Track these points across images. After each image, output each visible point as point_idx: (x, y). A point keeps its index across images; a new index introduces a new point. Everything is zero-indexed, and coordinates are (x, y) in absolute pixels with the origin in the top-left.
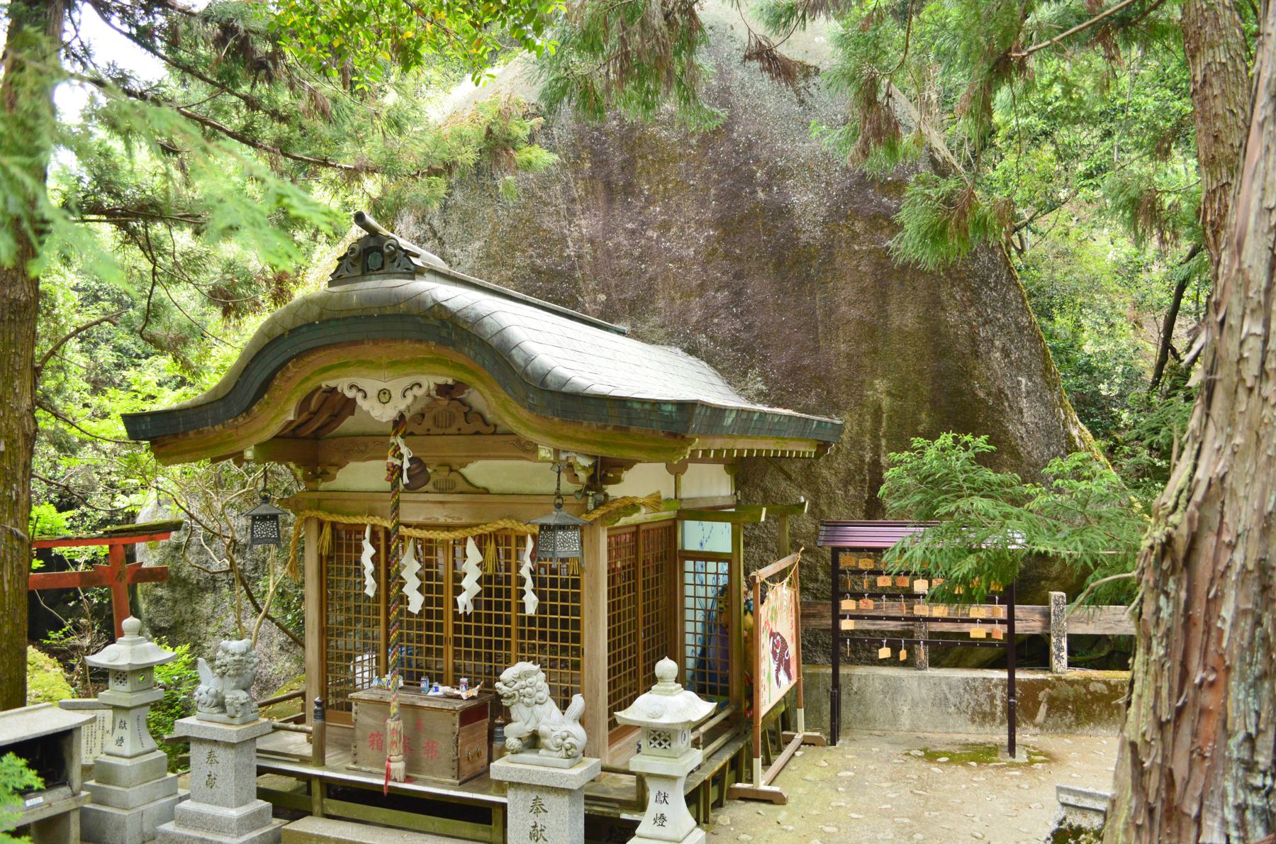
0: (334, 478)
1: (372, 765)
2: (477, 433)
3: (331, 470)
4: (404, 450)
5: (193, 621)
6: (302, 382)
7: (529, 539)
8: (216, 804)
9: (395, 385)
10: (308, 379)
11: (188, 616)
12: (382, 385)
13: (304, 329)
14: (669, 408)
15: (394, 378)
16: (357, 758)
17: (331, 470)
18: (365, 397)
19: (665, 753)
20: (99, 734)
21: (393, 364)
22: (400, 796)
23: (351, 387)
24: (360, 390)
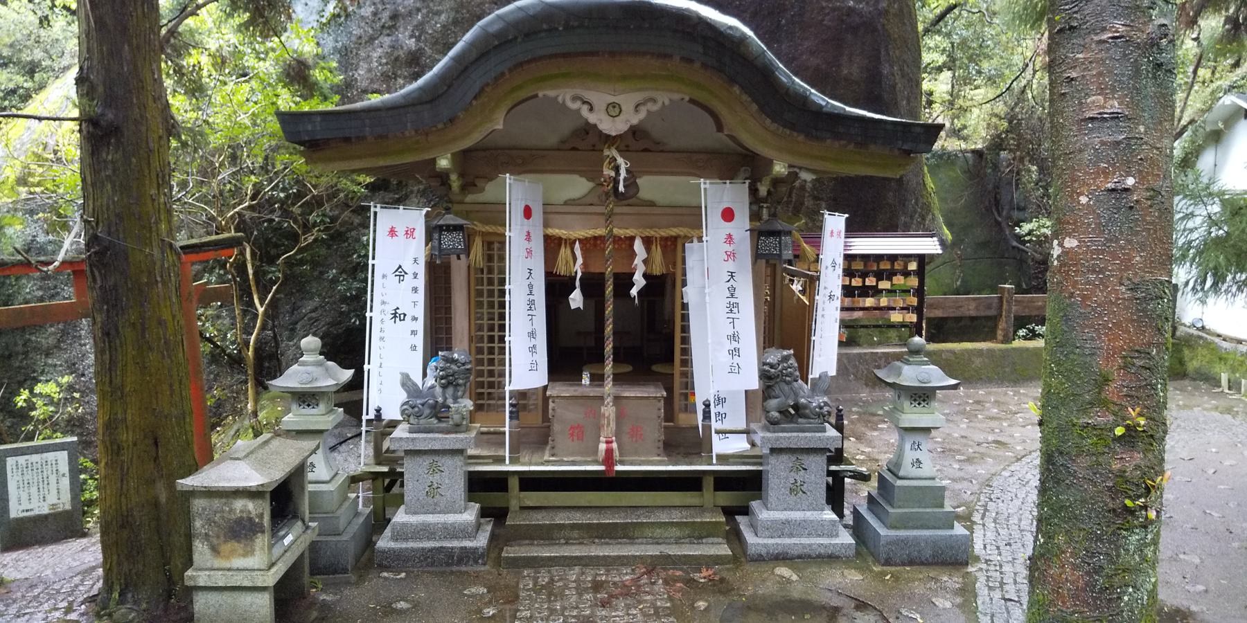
0: (482, 190)
1: (572, 455)
2: (646, 150)
3: (479, 183)
4: (620, 160)
5: (26, 353)
6: (514, 90)
7: (638, 246)
8: (439, 513)
9: (627, 100)
10: (520, 87)
11: (20, 348)
12: (611, 99)
13: (543, 34)
14: (918, 130)
15: (624, 92)
16: (555, 451)
17: (479, 183)
18: (591, 109)
19: (924, 410)
20: (53, 479)
21: (624, 78)
22: (635, 479)
23: (575, 98)
24: (584, 103)
